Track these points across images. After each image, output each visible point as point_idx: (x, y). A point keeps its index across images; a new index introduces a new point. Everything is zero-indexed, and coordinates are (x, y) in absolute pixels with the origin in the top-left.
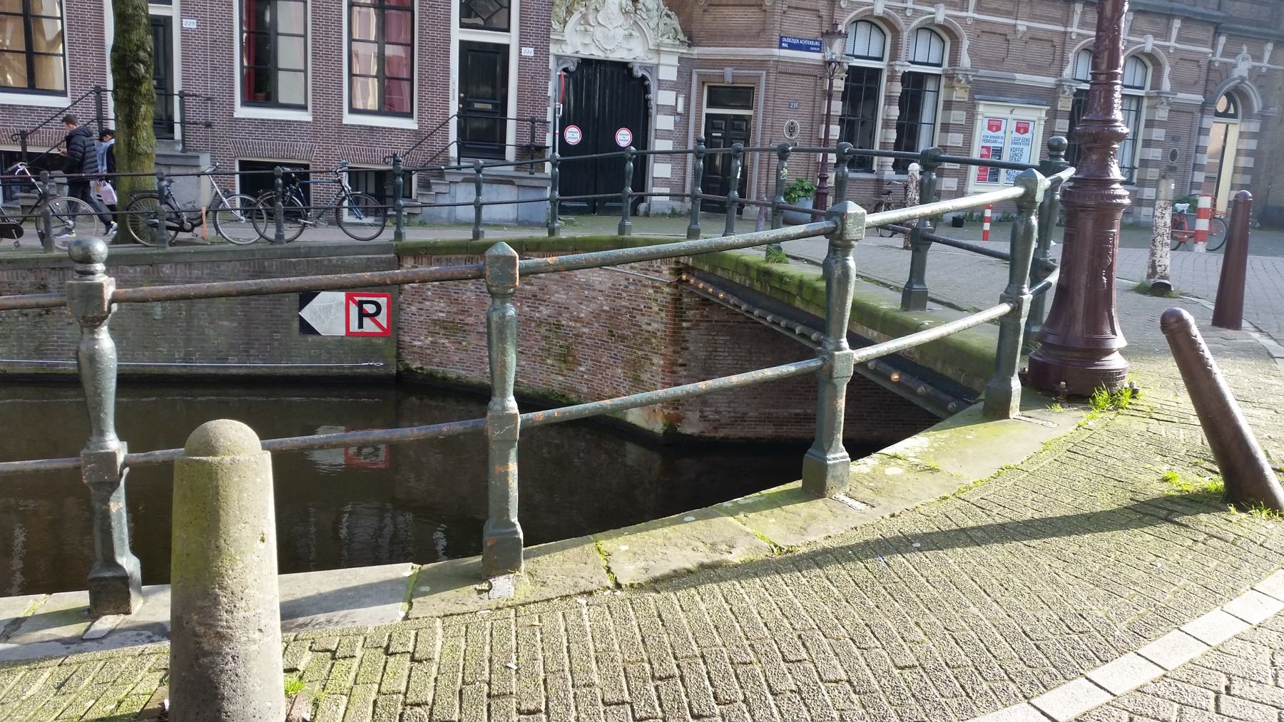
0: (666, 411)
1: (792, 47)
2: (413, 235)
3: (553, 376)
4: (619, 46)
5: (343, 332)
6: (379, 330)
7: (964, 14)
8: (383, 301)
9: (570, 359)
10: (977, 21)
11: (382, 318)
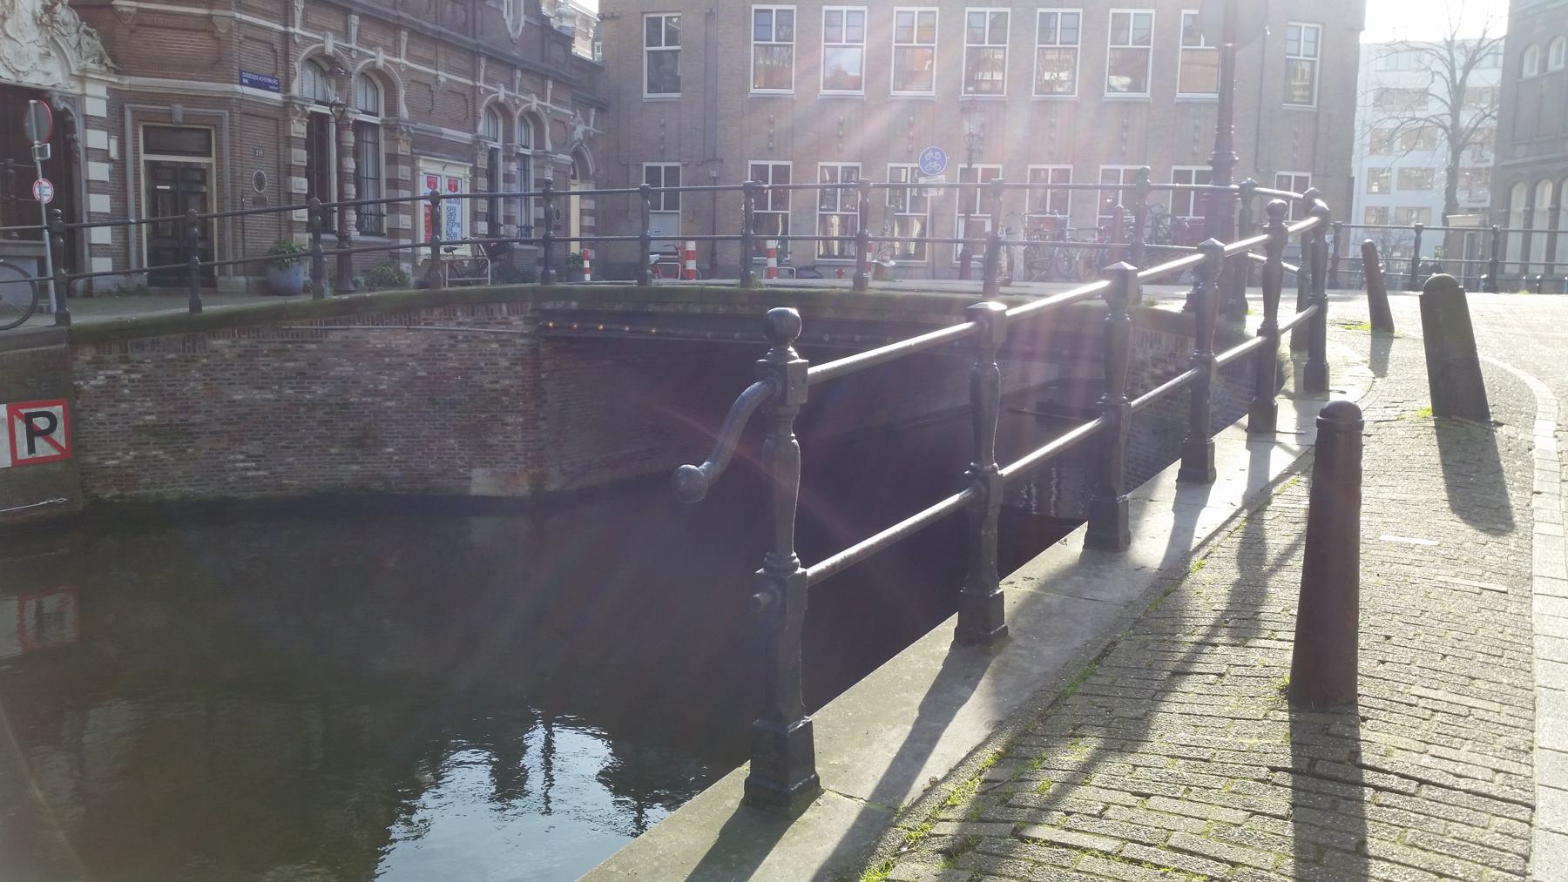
0: (531, 471)
1: (253, 84)
2: (210, 308)
3: (341, 467)
4: (34, 68)
5: (8, 463)
6: (55, 452)
7: (397, 60)
8: (57, 410)
9: (369, 441)
10: (409, 69)
11: (59, 436)
